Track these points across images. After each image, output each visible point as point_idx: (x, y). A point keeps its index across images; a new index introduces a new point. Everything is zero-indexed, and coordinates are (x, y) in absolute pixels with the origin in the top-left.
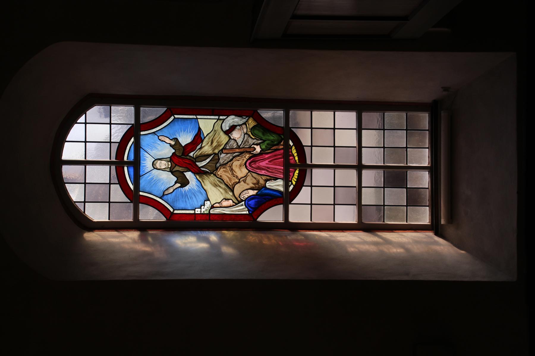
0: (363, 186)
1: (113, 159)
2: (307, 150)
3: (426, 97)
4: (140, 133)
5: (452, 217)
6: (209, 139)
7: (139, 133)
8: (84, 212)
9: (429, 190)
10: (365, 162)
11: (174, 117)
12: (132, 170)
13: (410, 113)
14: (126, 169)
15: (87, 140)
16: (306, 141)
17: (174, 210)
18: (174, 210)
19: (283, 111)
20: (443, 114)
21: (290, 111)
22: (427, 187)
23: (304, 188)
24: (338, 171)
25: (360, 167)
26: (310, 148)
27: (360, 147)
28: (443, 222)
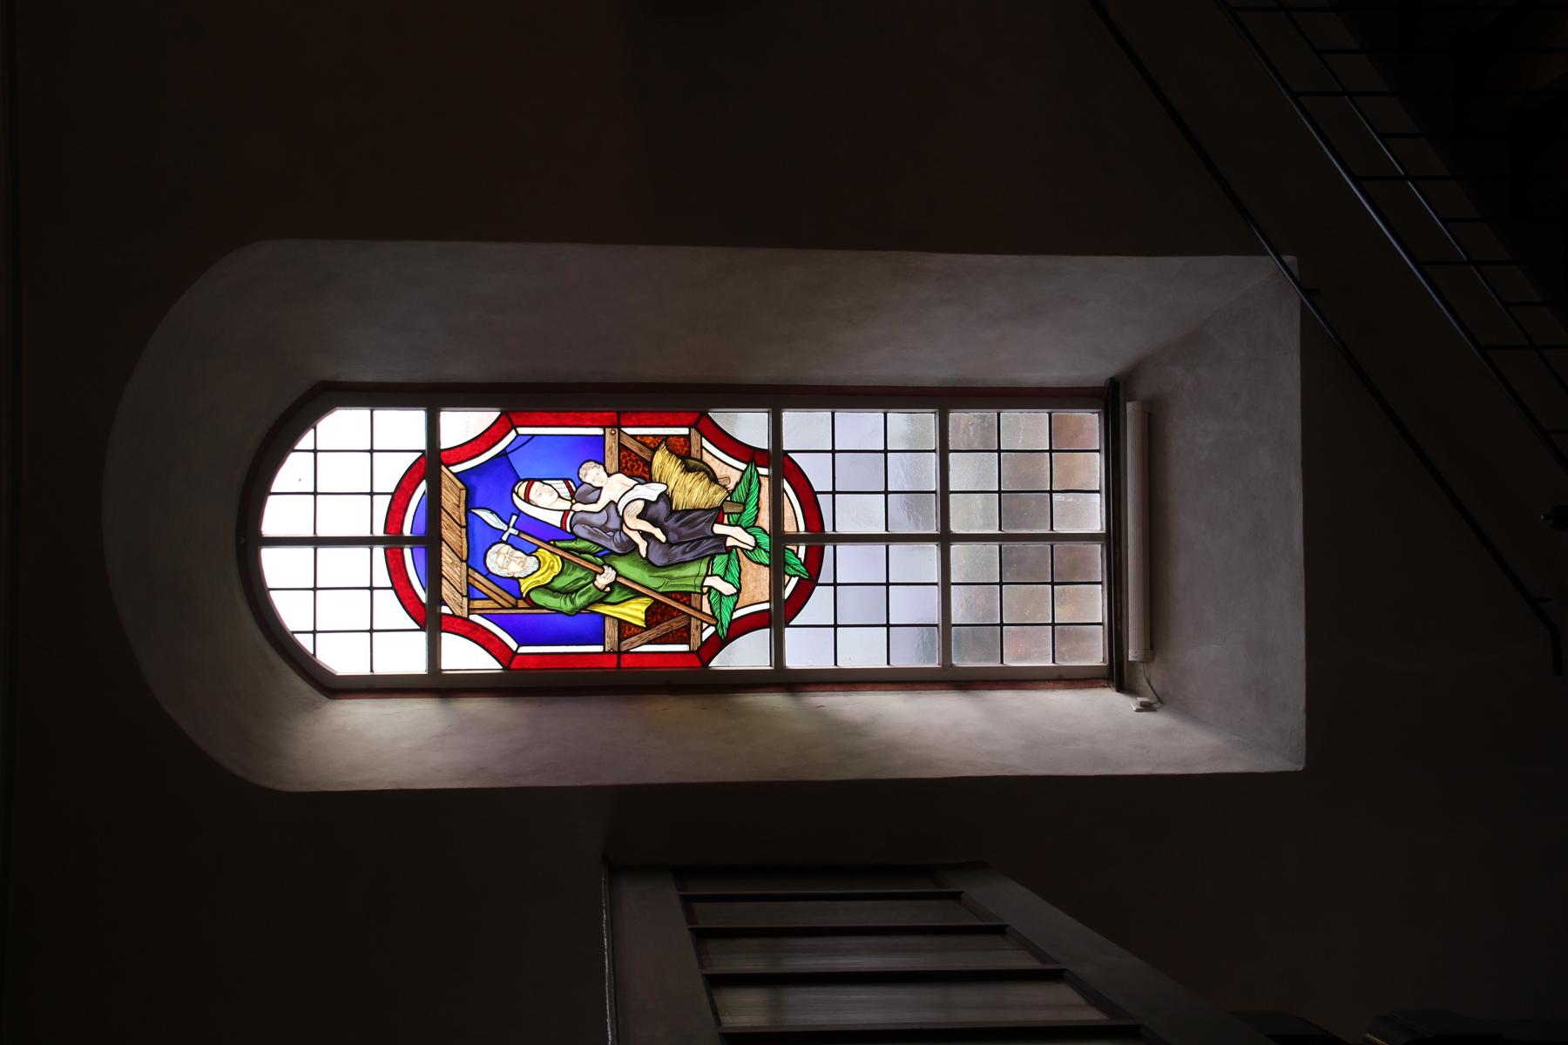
0: (953, 581)
1: (379, 531)
2: (824, 502)
3: (1096, 372)
4: (440, 609)
5: (1154, 641)
6: (600, 537)
7: (438, 608)
8: (314, 654)
9: (1104, 629)
10: (955, 528)
11: (517, 432)
12: (421, 553)
13: (1057, 413)
14: (407, 552)
15: (313, 491)
16: (820, 481)
17: (518, 435)
18: (518, 435)
19: (768, 412)
20: (1130, 406)
21: (783, 414)
22: (1101, 621)
23: (817, 588)
24: (894, 548)
25: (945, 539)
26: (838, 623)
27: (944, 451)
28: (1132, 655)
